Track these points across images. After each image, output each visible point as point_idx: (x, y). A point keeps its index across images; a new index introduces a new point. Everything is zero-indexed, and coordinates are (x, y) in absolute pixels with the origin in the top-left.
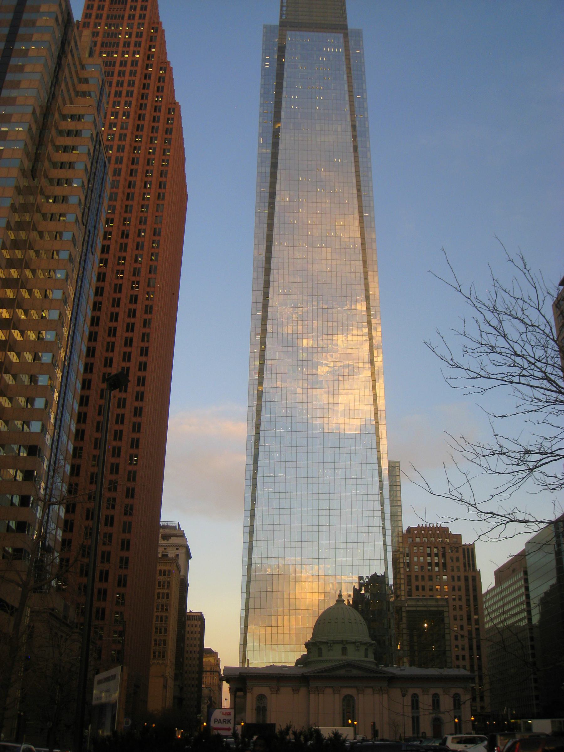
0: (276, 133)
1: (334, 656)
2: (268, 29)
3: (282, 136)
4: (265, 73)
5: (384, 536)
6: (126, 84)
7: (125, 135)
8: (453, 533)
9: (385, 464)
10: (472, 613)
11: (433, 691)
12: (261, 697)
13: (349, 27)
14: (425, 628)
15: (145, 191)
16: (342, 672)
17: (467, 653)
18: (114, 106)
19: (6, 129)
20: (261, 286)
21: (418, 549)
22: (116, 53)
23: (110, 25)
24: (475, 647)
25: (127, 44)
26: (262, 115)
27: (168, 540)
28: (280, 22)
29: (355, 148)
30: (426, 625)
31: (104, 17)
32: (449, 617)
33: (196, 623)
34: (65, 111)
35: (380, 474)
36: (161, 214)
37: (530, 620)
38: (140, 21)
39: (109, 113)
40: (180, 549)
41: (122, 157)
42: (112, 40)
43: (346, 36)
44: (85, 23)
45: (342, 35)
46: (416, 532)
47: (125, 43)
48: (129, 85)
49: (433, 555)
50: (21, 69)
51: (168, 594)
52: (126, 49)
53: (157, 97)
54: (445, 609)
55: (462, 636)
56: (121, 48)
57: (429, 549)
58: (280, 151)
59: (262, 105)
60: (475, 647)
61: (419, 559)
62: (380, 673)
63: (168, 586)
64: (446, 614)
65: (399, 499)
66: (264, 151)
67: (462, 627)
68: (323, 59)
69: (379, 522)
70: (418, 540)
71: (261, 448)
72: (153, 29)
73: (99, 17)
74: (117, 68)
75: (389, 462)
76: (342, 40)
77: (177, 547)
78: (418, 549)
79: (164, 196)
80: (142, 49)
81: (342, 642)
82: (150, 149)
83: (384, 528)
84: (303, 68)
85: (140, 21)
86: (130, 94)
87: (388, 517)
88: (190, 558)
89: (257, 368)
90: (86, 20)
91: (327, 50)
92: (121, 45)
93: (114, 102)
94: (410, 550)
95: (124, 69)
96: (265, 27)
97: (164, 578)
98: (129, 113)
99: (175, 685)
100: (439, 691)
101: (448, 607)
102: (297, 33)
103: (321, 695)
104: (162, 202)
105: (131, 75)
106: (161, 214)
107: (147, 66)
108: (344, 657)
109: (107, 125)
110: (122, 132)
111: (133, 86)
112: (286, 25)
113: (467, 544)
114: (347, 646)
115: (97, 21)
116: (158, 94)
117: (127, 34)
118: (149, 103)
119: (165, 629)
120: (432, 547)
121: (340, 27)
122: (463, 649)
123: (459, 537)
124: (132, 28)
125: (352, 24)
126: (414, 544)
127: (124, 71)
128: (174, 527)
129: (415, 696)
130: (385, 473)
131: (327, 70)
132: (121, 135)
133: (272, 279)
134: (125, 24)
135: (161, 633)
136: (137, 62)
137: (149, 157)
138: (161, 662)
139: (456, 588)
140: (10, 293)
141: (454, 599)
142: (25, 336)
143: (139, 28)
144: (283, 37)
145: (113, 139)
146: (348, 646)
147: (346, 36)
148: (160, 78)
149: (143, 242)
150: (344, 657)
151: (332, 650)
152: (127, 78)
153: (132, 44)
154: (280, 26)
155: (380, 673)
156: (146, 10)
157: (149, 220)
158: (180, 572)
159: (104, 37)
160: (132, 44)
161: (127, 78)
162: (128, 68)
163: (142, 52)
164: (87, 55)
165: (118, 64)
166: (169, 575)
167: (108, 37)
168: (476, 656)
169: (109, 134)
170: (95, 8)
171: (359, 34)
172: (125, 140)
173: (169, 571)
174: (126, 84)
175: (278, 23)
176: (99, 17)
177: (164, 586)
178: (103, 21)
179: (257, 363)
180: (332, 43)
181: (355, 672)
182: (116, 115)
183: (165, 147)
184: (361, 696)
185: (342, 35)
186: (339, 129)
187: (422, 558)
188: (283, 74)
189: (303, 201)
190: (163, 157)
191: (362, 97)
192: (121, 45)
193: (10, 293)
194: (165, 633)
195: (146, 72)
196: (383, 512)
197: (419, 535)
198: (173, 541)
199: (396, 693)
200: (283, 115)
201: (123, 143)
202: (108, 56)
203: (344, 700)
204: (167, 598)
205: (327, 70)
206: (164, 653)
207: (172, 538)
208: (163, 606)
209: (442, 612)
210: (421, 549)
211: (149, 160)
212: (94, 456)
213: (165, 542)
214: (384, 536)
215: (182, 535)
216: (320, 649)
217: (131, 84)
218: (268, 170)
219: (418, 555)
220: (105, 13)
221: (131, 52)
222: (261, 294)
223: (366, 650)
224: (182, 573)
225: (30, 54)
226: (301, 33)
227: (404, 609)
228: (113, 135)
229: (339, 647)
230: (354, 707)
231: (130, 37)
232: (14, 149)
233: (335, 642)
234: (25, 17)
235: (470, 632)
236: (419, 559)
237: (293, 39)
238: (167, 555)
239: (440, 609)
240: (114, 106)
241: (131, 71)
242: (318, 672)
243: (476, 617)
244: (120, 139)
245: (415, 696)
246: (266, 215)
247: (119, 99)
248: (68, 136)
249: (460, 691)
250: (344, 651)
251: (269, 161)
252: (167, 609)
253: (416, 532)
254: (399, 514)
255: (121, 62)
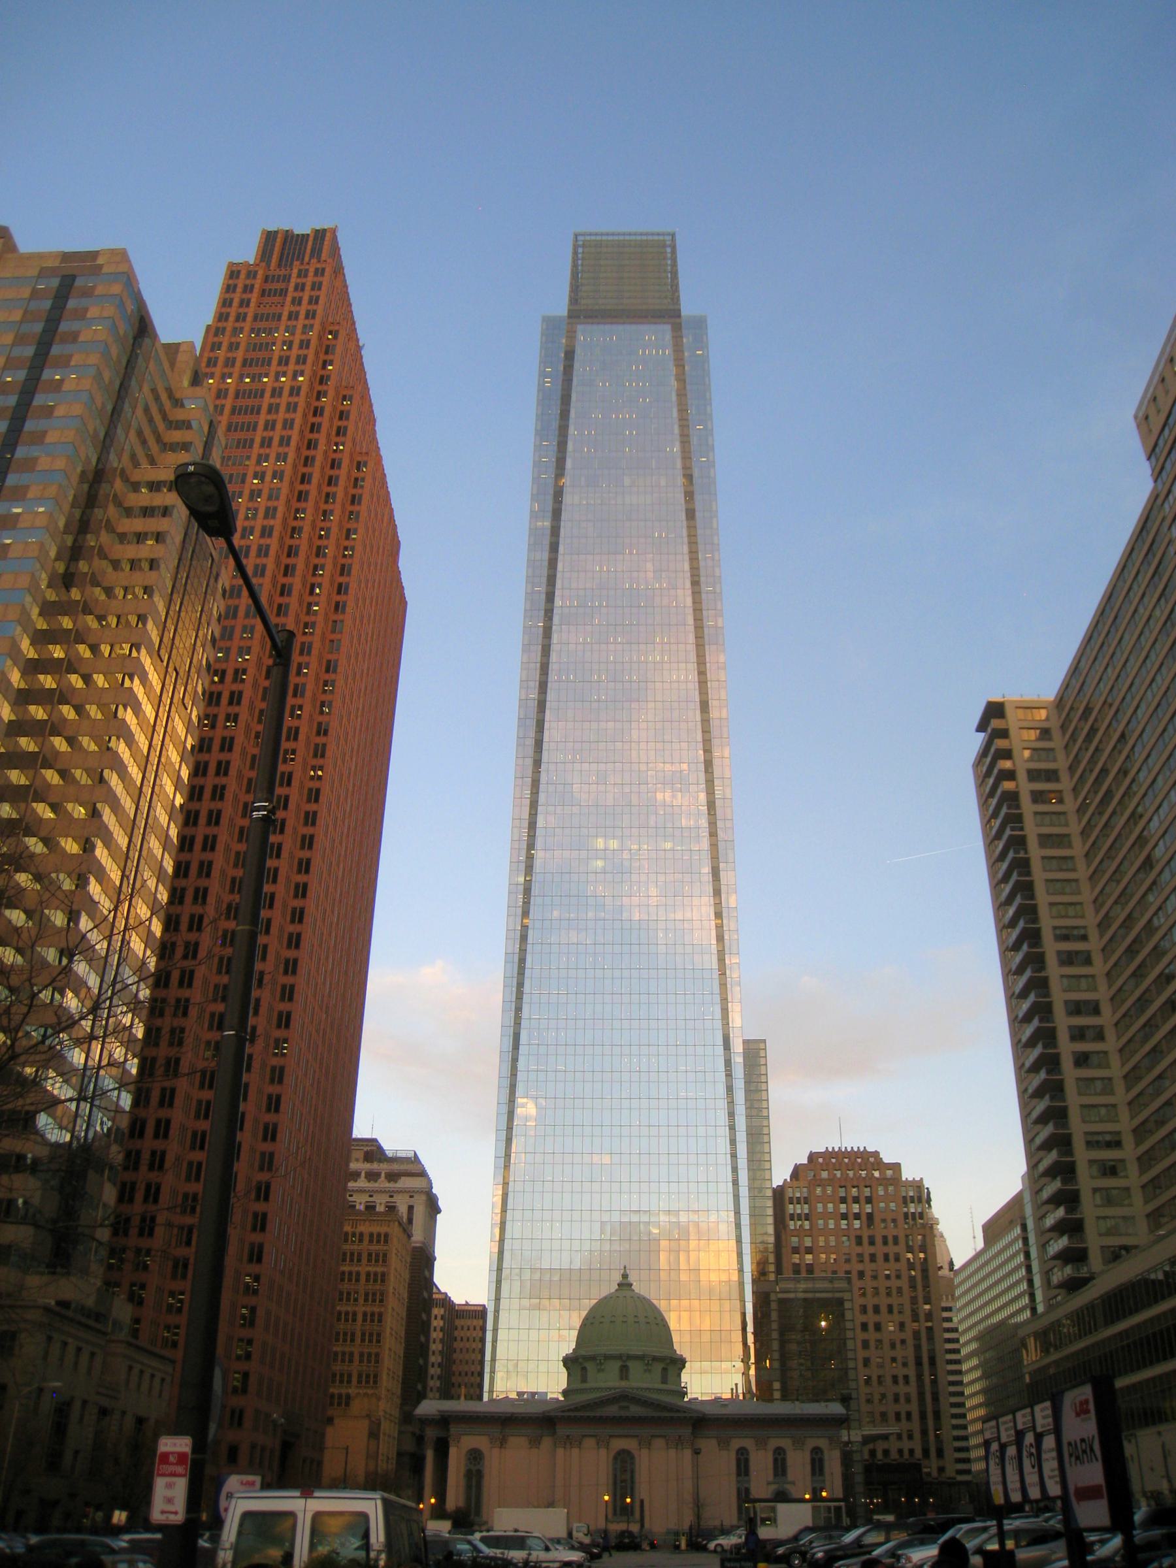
0: (558, 494)
1: (607, 1380)
2: (550, 323)
3: (567, 499)
4: (544, 396)
5: (735, 1170)
6: (279, 426)
7: (275, 509)
8: (886, 1161)
9: (738, 1047)
10: (921, 1299)
11: (811, 1443)
12: (475, 1456)
13: (683, 313)
14: (820, 1329)
15: (311, 599)
16: (612, 1410)
17: (911, 1372)
18: (259, 463)
19: (19, 510)
20: (530, 751)
21: (824, 1191)
22: (284, 376)
23: (259, 329)
24: (925, 1360)
25: (284, 361)
26: (537, 464)
27: (396, 1182)
28: (569, 311)
29: (691, 514)
30: (823, 1323)
31: (249, 318)
32: (852, 1309)
33: (475, 1322)
34: (136, 476)
35: (728, 1063)
36: (339, 636)
37: (1034, 1310)
38: (307, 322)
39: (250, 473)
40: (416, 1196)
41: (268, 546)
42: (260, 355)
43: (677, 329)
44: (217, 329)
45: (668, 327)
46: (821, 1160)
47: (281, 358)
48: (284, 428)
49: (850, 1200)
50: (48, 412)
51: (383, 1275)
52: (282, 369)
53: (337, 444)
54: (847, 1296)
55: (903, 1342)
56: (274, 366)
57: (868, 1189)
58: (562, 524)
59: (538, 448)
60: (925, 1360)
61: (825, 1207)
62: (678, 1411)
63: (384, 1261)
64: (847, 1305)
65: (764, 1105)
66: (540, 524)
67: (902, 1325)
68: (637, 367)
69: (724, 1146)
70: (825, 1175)
71: (524, 1023)
72: (330, 333)
73: (241, 318)
74: (267, 400)
75: (746, 1042)
76: (668, 336)
77: (411, 1193)
78: (824, 1191)
79: (344, 606)
80: (308, 368)
81: (619, 1357)
82: (322, 529)
83: (734, 1156)
84: (604, 385)
85: (307, 322)
86: (285, 441)
87: (742, 1137)
88: (439, 1211)
89: (521, 888)
90: (220, 325)
91: (644, 353)
92: (275, 362)
93: (260, 456)
94: (809, 1191)
95: (278, 401)
96: (546, 320)
97: (377, 1247)
98: (282, 472)
99: (400, 1432)
100: (748, 1443)
101: (850, 1291)
102: (595, 327)
103: (575, 1451)
104: (341, 617)
105: (288, 410)
106: (339, 636)
107: (319, 395)
108: (624, 1384)
109: (246, 493)
110: (270, 504)
111: (291, 428)
112: (582, 311)
113: (910, 1179)
114: (630, 1364)
115: (237, 325)
116: (337, 440)
117: (284, 343)
118: (319, 455)
119: (379, 1335)
120: (849, 1186)
121: (670, 314)
122: (905, 1365)
123: (896, 1167)
124: (293, 334)
125: (688, 308)
126: (817, 1182)
127: (278, 405)
128: (406, 1160)
129: (779, 1453)
130: (738, 1060)
131: (644, 385)
132: (267, 509)
133: (546, 739)
134: (282, 328)
135: (370, 1341)
136: (299, 388)
137: (319, 543)
138: (370, 1391)
139: (891, 1257)
140: (16, 777)
141: (888, 1277)
142: (113, 847)
143: (303, 333)
144: (571, 335)
145: (255, 516)
146: (631, 1364)
147: (677, 329)
148: (342, 413)
149: (304, 685)
150: (624, 1384)
151: (603, 1370)
152: (281, 415)
153: (293, 360)
154: (570, 317)
155: (678, 1411)
156: (317, 303)
157: (316, 646)
158: (409, 1236)
159: (247, 351)
160: (293, 360)
161: (281, 415)
162: (285, 399)
163: (308, 372)
164: (186, 383)
165: (268, 394)
166: (386, 1241)
167: (254, 350)
168: (927, 1379)
169: (248, 509)
170: (236, 303)
171: (700, 323)
172: (274, 517)
173: (386, 1235)
174: (279, 426)
175: (565, 313)
176: (241, 318)
177: (377, 1261)
178: (247, 326)
179: (521, 879)
180: (653, 340)
181: (636, 1410)
182: (261, 476)
183: (349, 526)
184: (645, 1452)
185: (668, 327)
186: (663, 483)
187: (830, 1206)
188: (570, 396)
189: (600, 606)
190: (347, 543)
191: (705, 428)
192: (275, 362)
193: (16, 777)
194: (378, 1341)
195: (317, 404)
196: (732, 1128)
197: (826, 1166)
198: (405, 1183)
199: (708, 1445)
200: (569, 464)
201: (272, 522)
202: (252, 381)
203: (615, 1458)
204: (383, 1281)
205: (644, 385)
206: (376, 1376)
207: (403, 1178)
208: (374, 1294)
209: (841, 1302)
210: (829, 1190)
211: (319, 548)
212: (208, 1043)
213: (391, 1185)
214: (735, 1170)
215: (423, 1174)
216: (584, 1369)
217: (288, 424)
218: (546, 556)
219: (824, 1200)
220: (251, 311)
221: (290, 373)
222: (529, 762)
223: (665, 1370)
224: (418, 1236)
225: (66, 387)
226: (601, 327)
227: (773, 1297)
228: (256, 509)
229: (615, 1366)
230: (632, 1472)
231: (290, 348)
232: (27, 543)
233: (607, 1357)
234: (64, 327)
235: (916, 1335)
236: (825, 1207)
237: (589, 336)
238: (374, 1207)
239: (838, 1295)
240: (259, 463)
241: (289, 404)
242: (569, 1411)
243: (927, 1307)
244: (266, 517)
245: (816, 1451)
246: (541, 629)
247: (268, 451)
248: (164, 515)
249: (822, 1443)
250: (624, 1372)
251: (546, 542)
252: (381, 1301)
253: (821, 1160)
254: (765, 1131)
255: (274, 390)
